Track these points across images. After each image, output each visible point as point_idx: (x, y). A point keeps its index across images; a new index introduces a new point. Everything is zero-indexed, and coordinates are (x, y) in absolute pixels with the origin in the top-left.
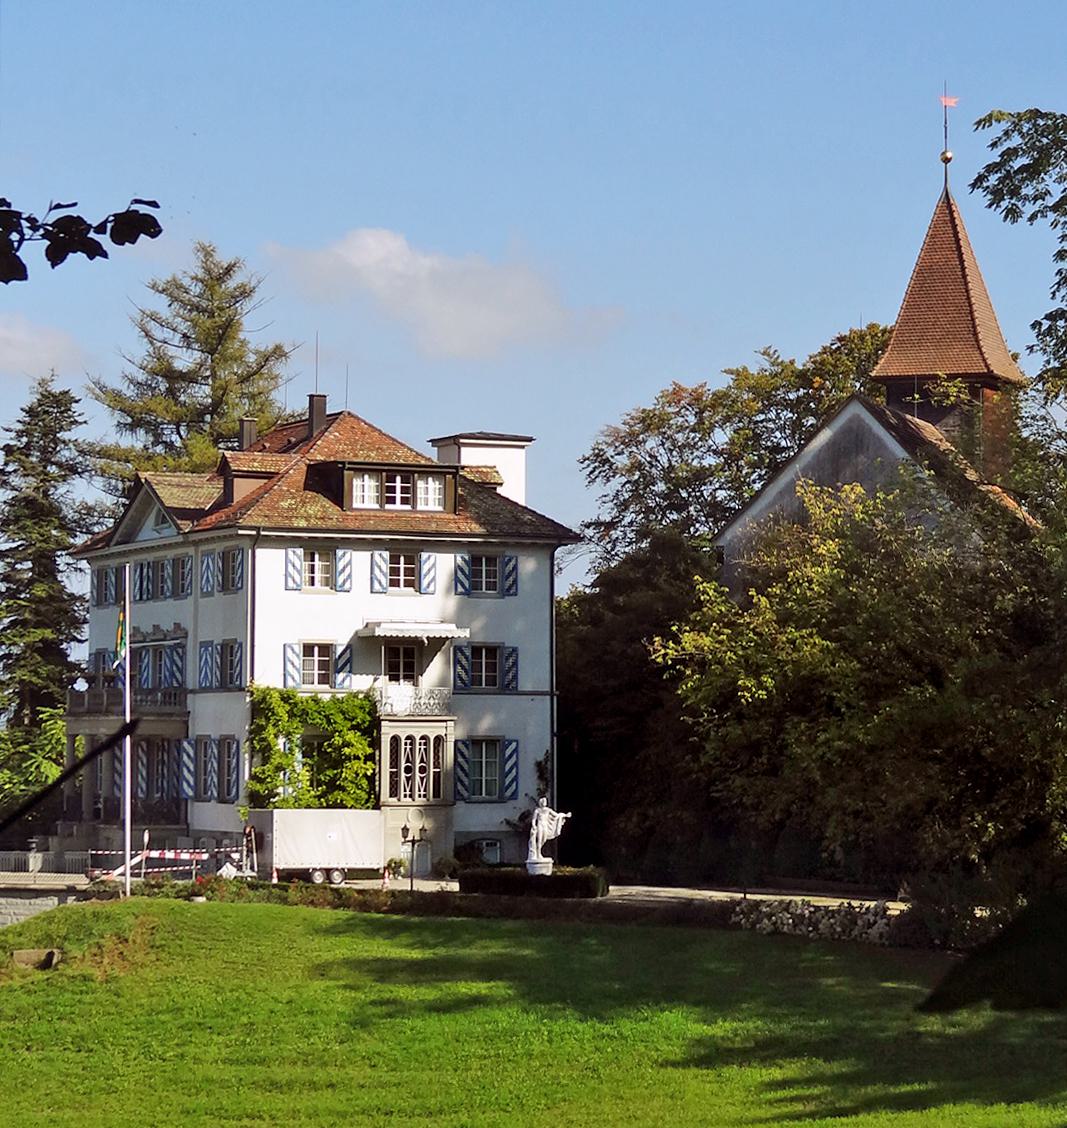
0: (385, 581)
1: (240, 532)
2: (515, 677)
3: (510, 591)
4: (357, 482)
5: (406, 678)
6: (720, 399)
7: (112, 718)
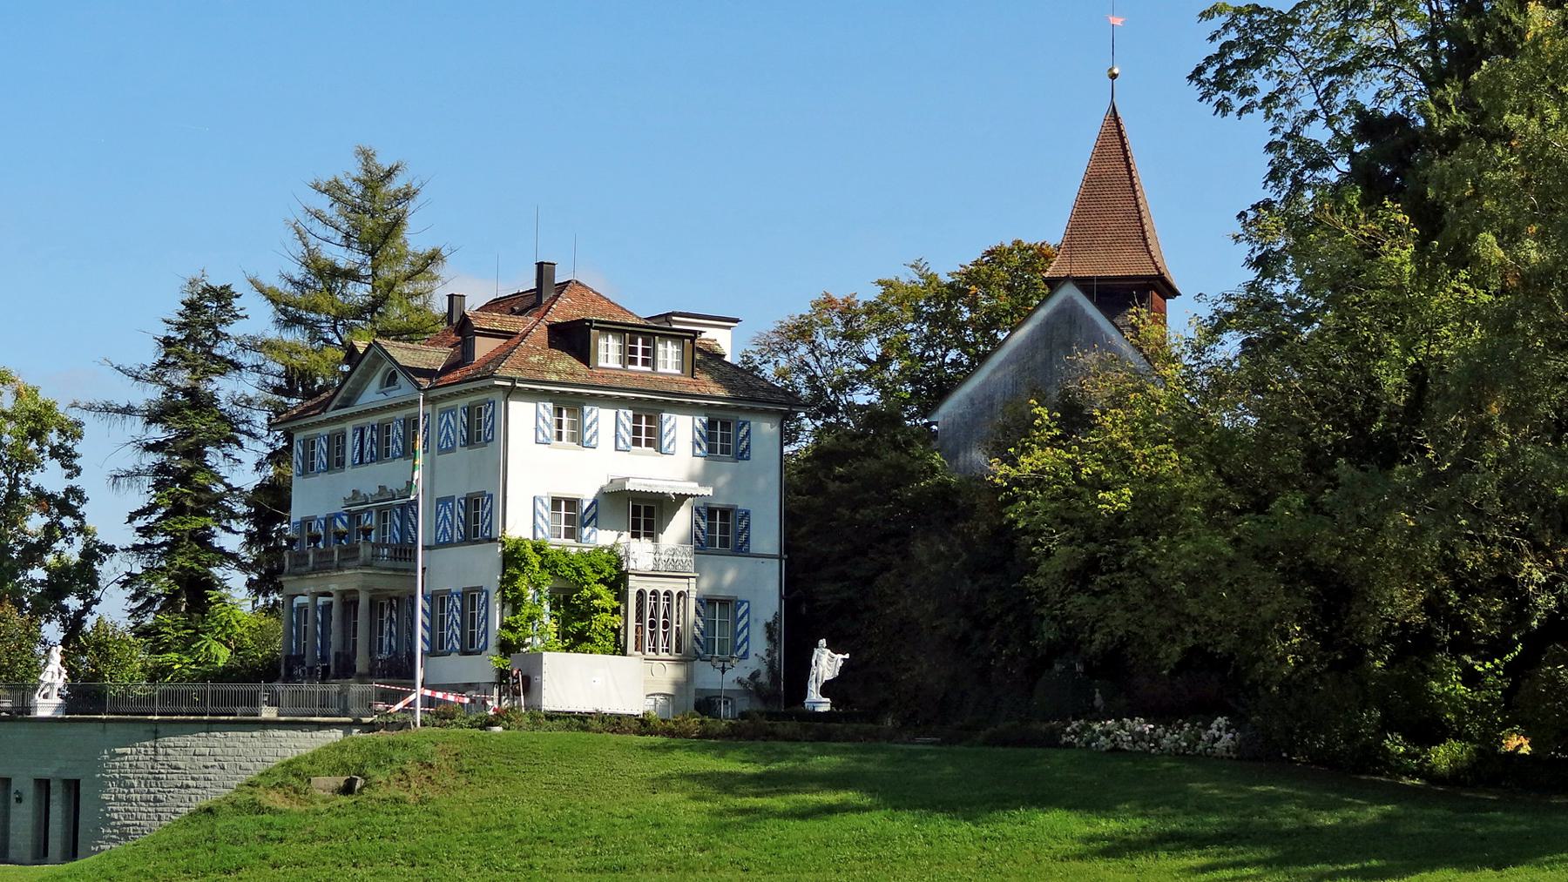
0: (629, 440)
1: (496, 383)
2: (747, 539)
3: (742, 455)
4: (602, 342)
5: (646, 535)
6: (870, 310)
7: (346, 572)
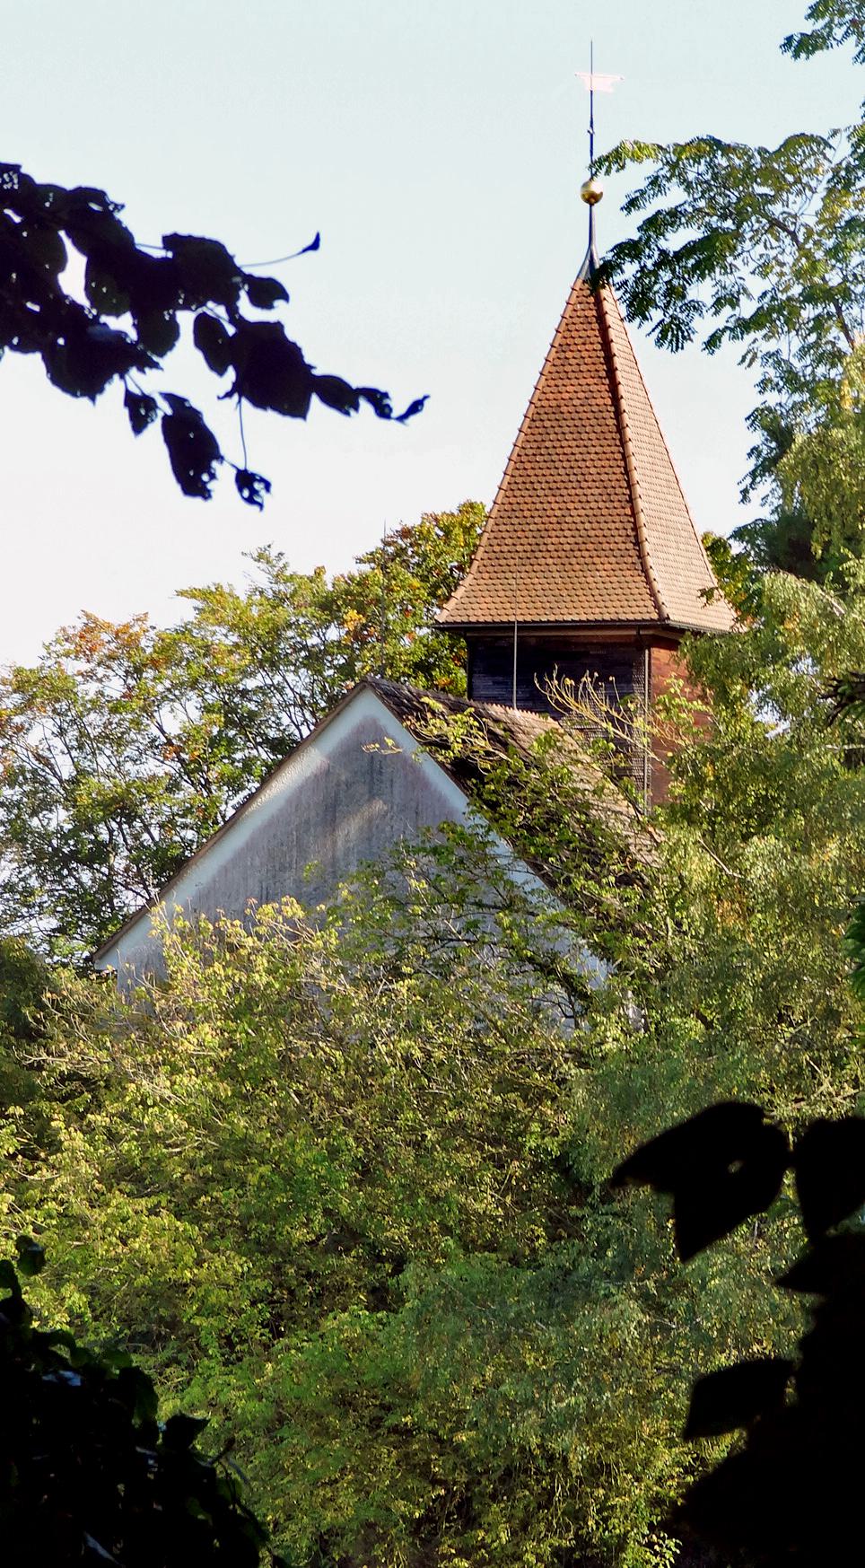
6: (167, 653)
